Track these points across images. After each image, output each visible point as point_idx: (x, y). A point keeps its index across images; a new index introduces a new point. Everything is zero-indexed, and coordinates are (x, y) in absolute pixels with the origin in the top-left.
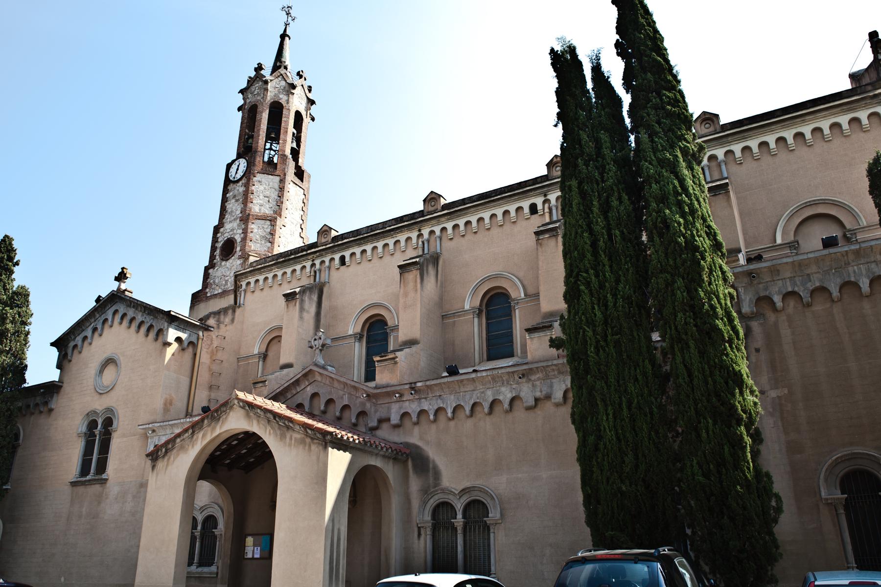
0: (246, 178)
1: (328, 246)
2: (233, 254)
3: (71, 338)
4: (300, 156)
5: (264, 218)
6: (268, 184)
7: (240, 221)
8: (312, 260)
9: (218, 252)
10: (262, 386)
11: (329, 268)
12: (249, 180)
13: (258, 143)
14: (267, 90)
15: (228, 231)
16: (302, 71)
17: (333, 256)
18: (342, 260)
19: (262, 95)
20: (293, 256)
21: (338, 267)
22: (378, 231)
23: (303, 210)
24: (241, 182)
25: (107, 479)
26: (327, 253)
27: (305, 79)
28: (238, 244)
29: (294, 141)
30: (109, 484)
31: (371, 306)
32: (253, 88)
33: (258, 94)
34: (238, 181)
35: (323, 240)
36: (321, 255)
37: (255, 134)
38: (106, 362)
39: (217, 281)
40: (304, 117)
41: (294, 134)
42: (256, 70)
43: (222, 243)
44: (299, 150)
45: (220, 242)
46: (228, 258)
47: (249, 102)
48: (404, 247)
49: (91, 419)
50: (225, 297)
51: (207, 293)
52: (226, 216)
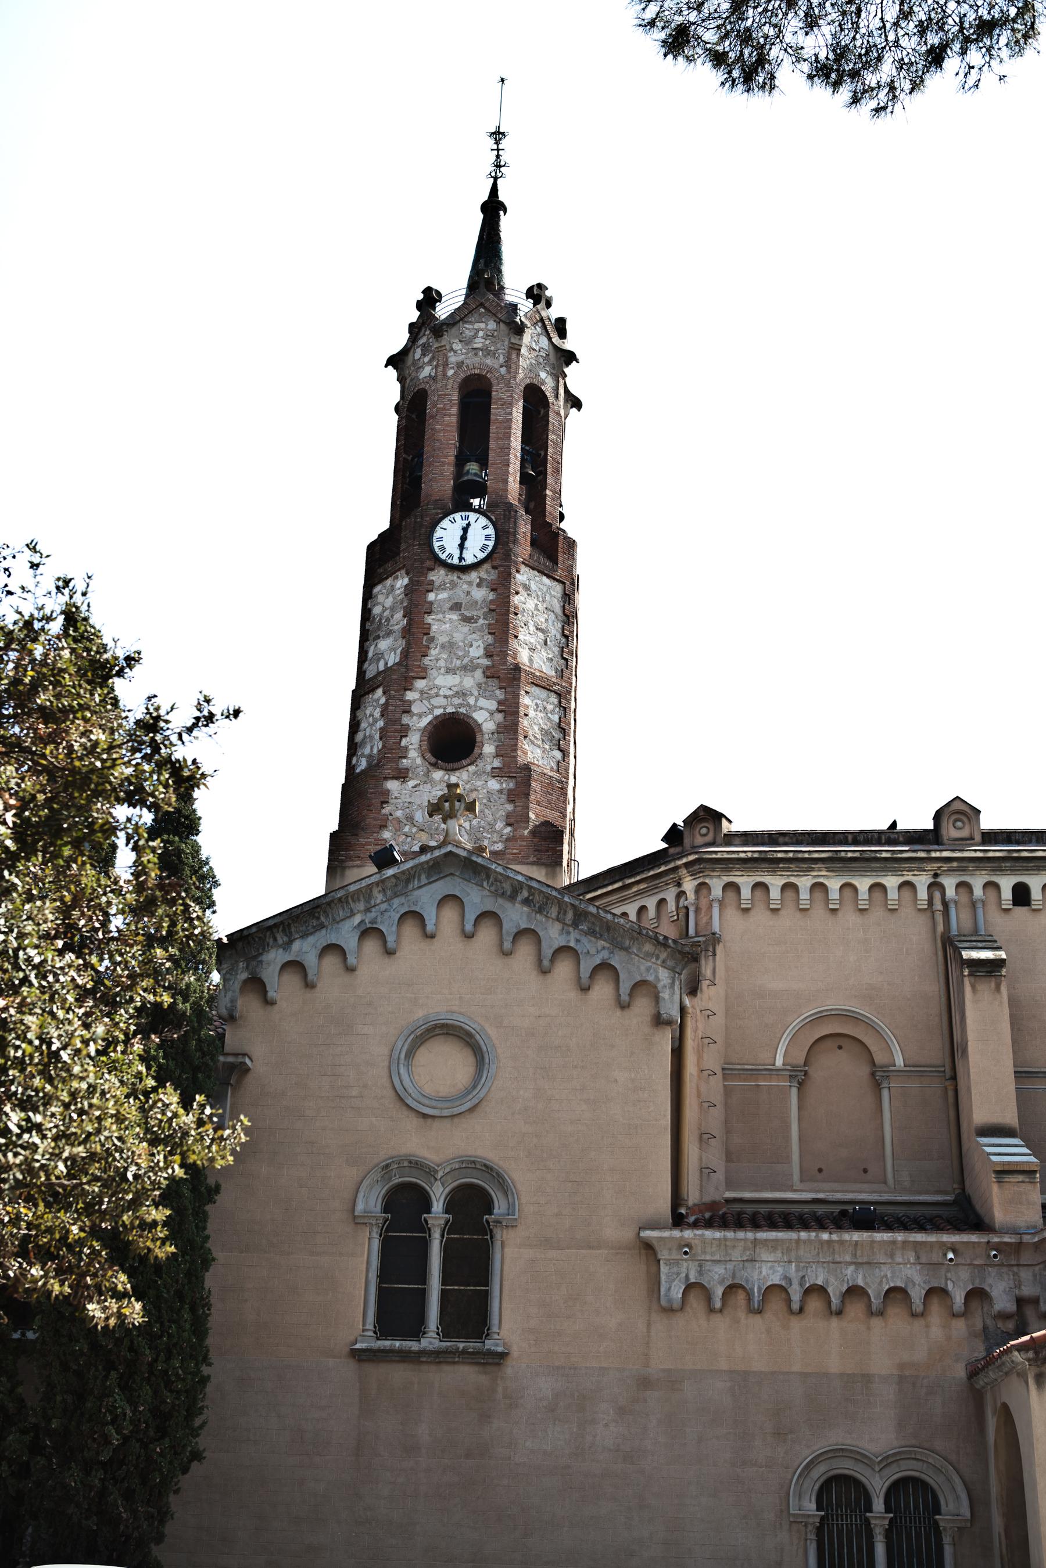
3: (275, 940)
5: (541, 684)
8: (932, 873)
10: (1023, 1182)
18: (1021, 895)
25: (507, 1354)
26: (978, 869)
30: (510, 1368)
36: (963, 870)
38: (428, 1030)
49: (396, 1180)
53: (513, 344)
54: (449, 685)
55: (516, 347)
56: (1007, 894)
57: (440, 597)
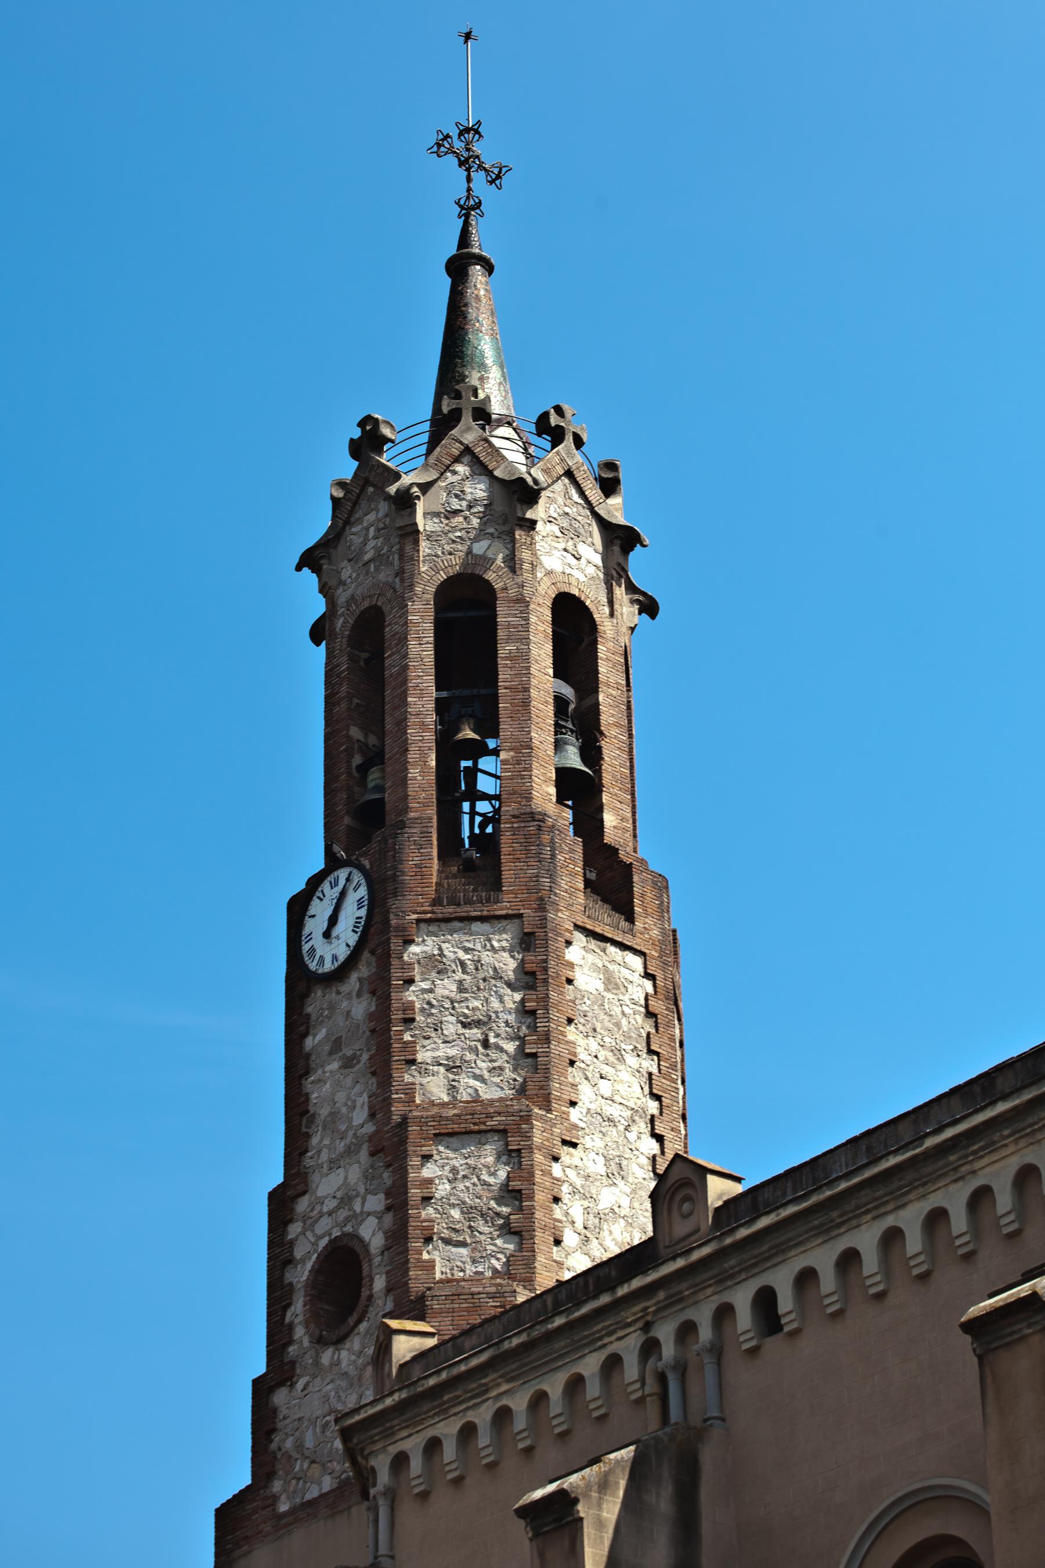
0: (372, 952)
1: (696, 1256)
2: (359, 1309)
4: (605, 798)
6: (471, 966)
7: (372, 1154)
8: (640, 1324)
9: (298, 1309)
11: (717, 1350)
12: (385, 960)
13: (404, 781)
14: (413, 532)
15: (330, 1205)
16: (559, 410)
17: (726, 1297)
19: (396, 562)
20: (559, 1321)
21: (753, 1343)
22: (893, 1161)
23: (651, 1052)
24: (354, 976)
27: (579, 442)
28: (377, 1260)
29: (570, 738)
31: (907, 1504)
32: (354, 536)
33: (379, 558)
34: (341, 973)
35: (681, 1228)
36: (676, 1301)
37: (390, 748)
39: (309, 1442)
40: (600, 613)
41: (560, 703)
42: (356, 449)
43: (309, 1265)
44: (598, 772)
45: (303, 1261)
46: (343, 1330)
47: (348, 604)
48: (1012, 1217)
50: (349, 1508)
51: (275, 1498)
52: (315, 1141)
53: (401, 528)
54: (331, 1191)
55: (409, 529)
56: (744, 1318)
57: (318, 1038)
